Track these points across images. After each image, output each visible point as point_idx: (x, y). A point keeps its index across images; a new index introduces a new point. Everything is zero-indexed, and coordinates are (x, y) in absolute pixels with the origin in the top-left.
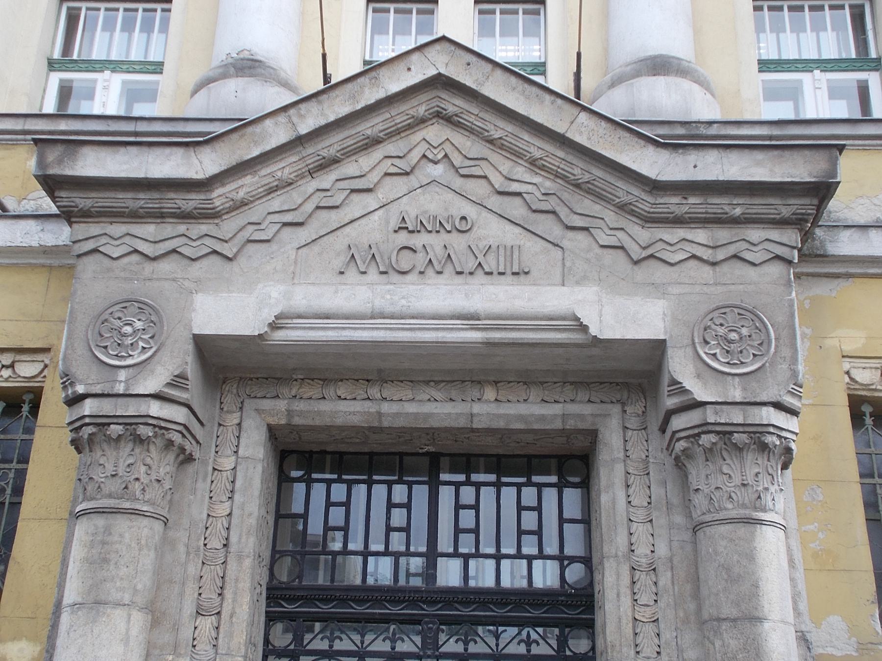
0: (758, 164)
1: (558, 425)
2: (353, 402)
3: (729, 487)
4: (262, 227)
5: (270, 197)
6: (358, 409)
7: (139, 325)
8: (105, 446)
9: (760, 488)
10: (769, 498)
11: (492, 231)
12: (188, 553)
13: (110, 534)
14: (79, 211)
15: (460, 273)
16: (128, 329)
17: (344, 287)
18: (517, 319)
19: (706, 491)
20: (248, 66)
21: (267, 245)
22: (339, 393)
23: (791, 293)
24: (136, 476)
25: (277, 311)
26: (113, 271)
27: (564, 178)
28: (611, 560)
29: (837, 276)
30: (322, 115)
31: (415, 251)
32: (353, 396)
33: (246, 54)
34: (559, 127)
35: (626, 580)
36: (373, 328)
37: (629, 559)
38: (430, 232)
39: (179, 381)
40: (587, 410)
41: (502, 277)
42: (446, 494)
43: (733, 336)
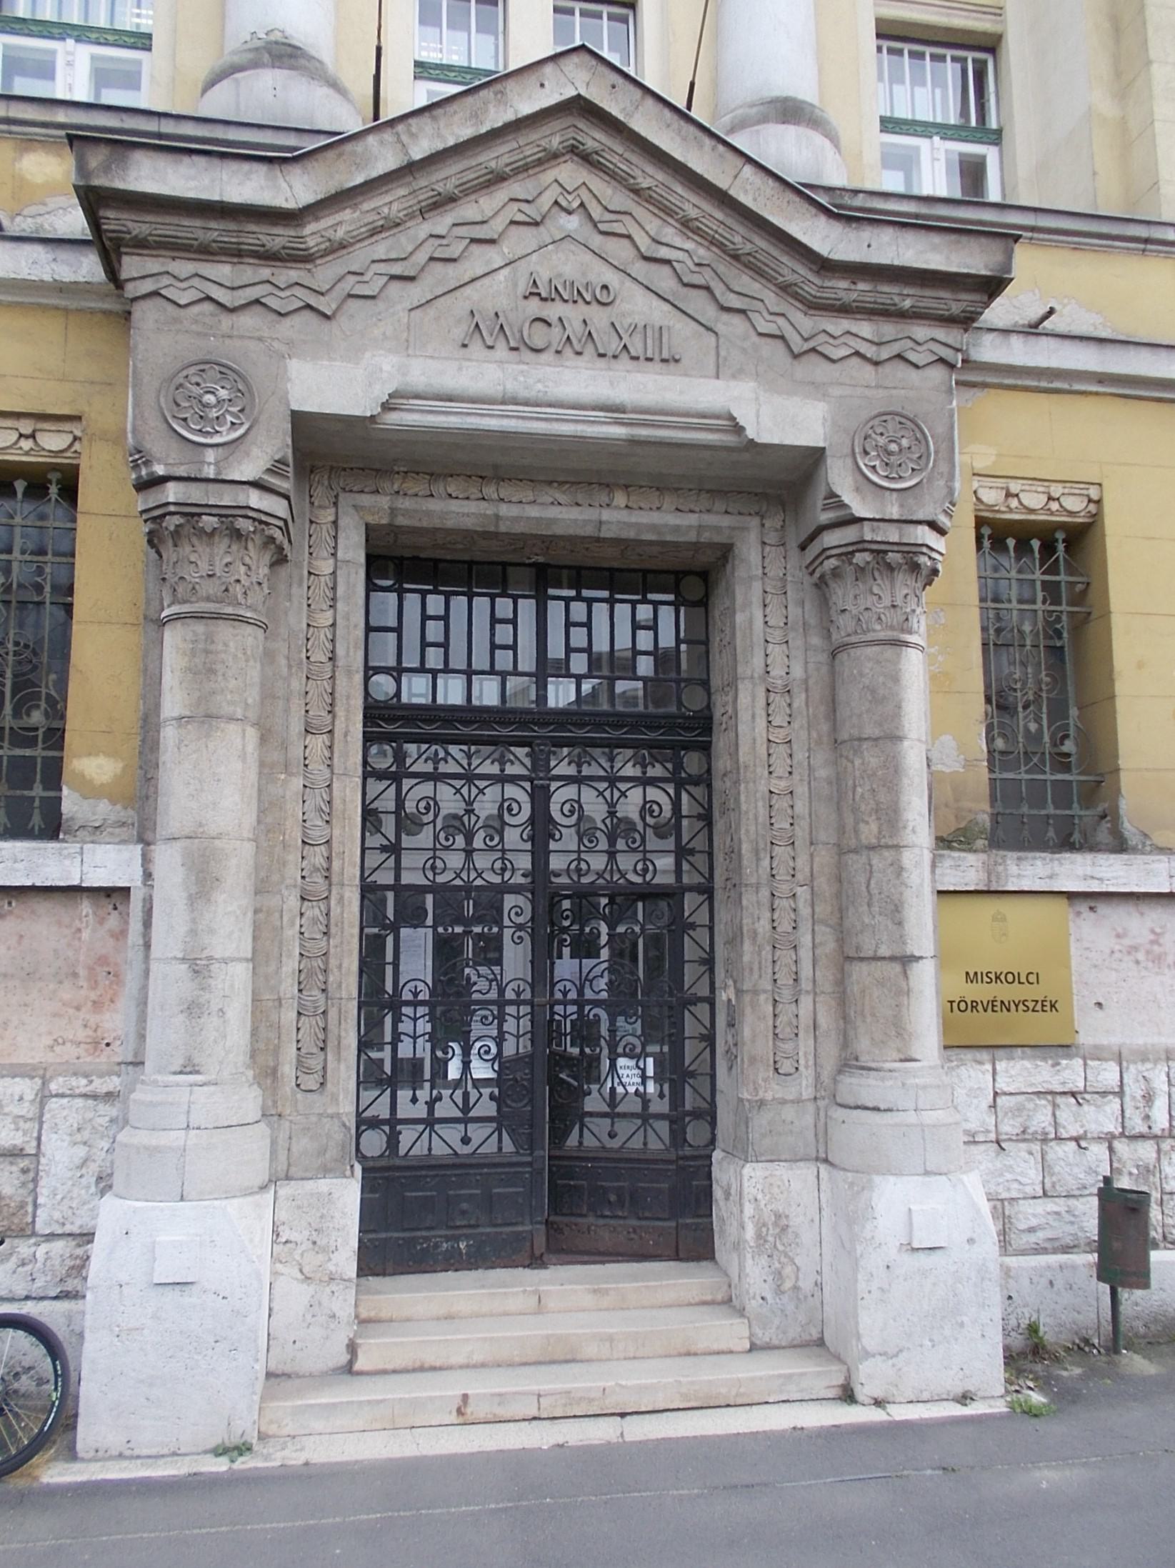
0: (935, 248)
1: (692, 537)
2: (466, 502)
3: (879, 608)
4: (366, 278)
5: (373, 239)
6: (473, 510)
7: (223, 394)
8: (195, 540)
9: (908, 610)
10: (915, 620)
11: (637, 306)
12: (290, 667)
13: (213, 642)
14: (131, 239)
15: (602, 355)
16: (210, 398)
17: (468, 363)
18: (667, 414)
19: (854, 612)
20: (283, 54)
21: (369, 302)
22: (450, 491)
23: (951, 403)
24: (237, 577)
25: (390, 389)
26: (181, 322)
27: (721, 246)
28: (746, 681)
29: (985, 385)
30: (439, 136)
31: (549, 325)
32: (466, 495)
33: (276, 36)
34: (722, 182)
35: (761, 702)
36: (502, 416)
37: (765, 680)
38: (566, 301)
39: (276, 469)
40: (726, 521)
41: (649, 363)
42: (555, 610)
43: (893, 447)
